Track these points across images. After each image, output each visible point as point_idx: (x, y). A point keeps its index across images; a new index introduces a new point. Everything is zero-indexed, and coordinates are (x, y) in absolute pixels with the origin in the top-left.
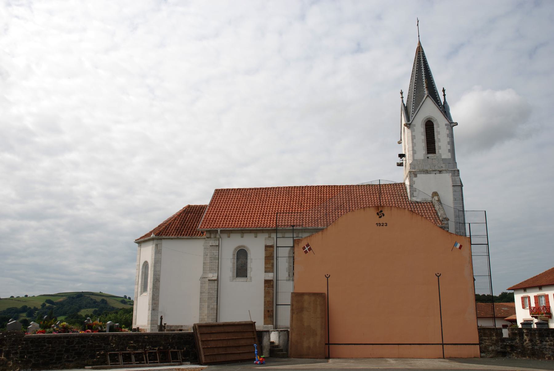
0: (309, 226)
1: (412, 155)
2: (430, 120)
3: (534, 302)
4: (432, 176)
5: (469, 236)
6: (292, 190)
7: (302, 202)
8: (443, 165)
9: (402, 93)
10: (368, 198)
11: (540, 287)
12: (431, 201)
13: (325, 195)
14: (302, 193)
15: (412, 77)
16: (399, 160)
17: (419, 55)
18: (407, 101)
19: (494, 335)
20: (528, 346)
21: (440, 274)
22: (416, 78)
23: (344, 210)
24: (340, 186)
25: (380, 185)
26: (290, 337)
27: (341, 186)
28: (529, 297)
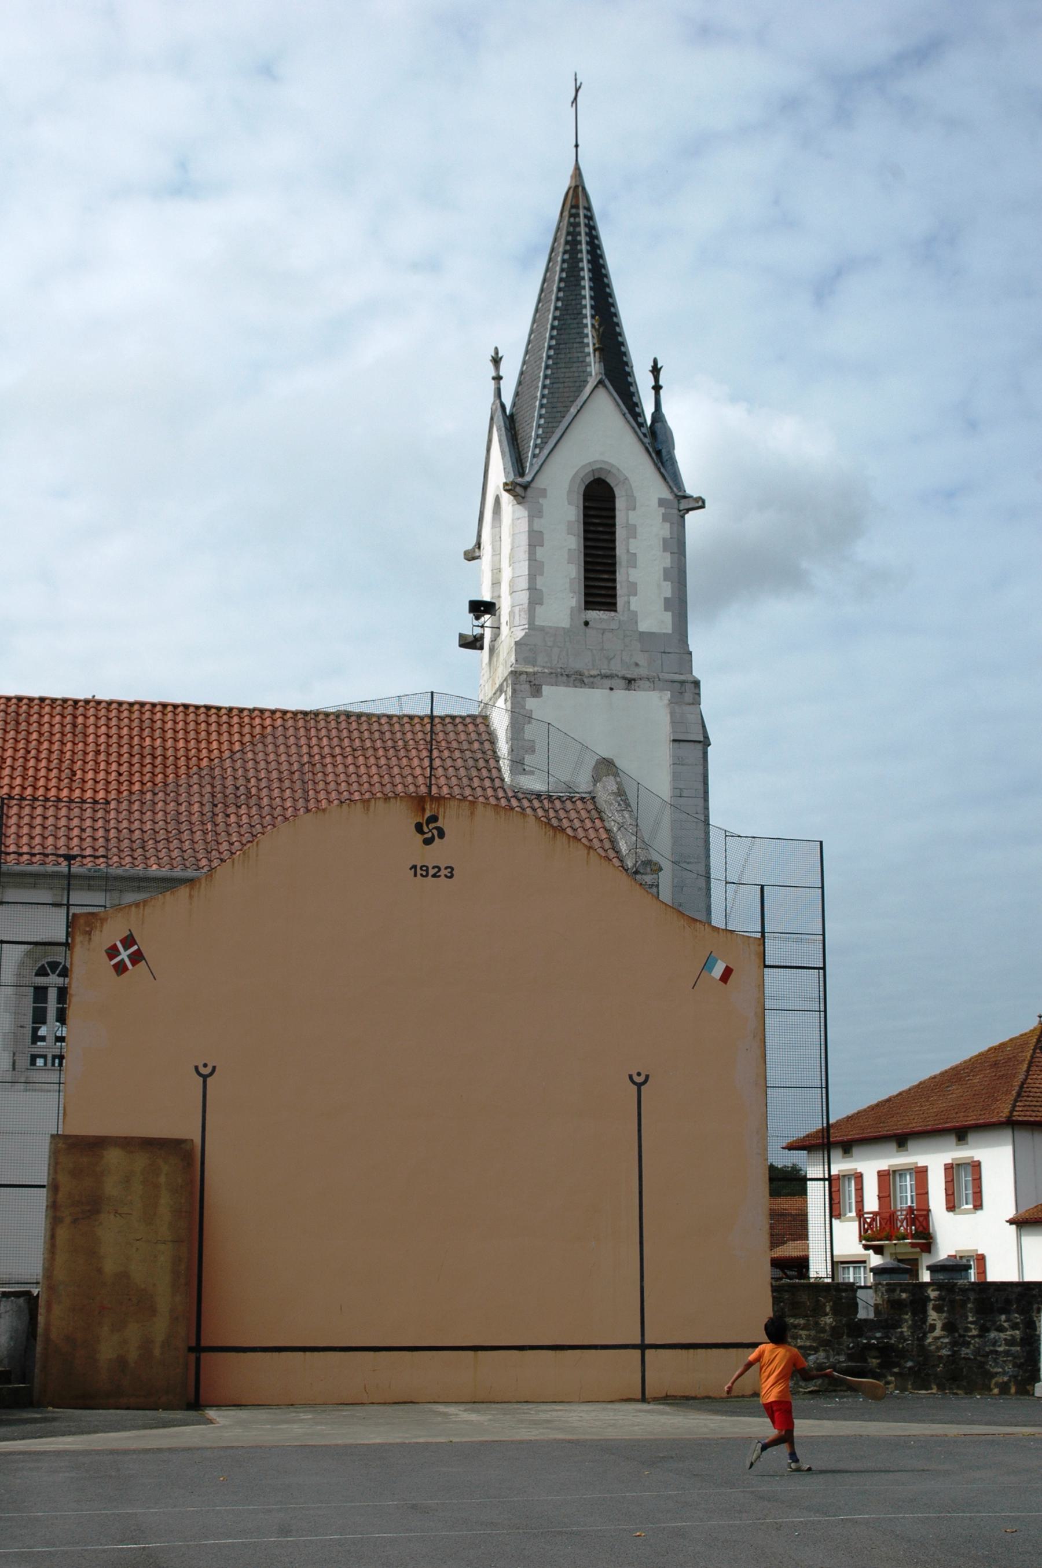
0: (110, 862)
1: (526, 606)
2: (603, 477)
3: (877, 1194)
4: (598, 695)
5: (759, 935)
6: (32, 711)
7: (73, 762)
8: (642, 659)
9: (496, 361)
10: (346, 767)
11: (902, 1141)
12: (590, 793)
13: (170, 743)
14: (74, 726)
15: (539, 301)
16: (468, 624)
17: (572, 220)
18: (517, 394)
19: (828, 1309)
20: (939, 1349)
21: (647, 1077)
22: (556, 308)
23: (249, 808)
24: (231, 709)
25: (432, 717)
26: (41, 1319)
27: (235, 712)
28: (859, 1177)
